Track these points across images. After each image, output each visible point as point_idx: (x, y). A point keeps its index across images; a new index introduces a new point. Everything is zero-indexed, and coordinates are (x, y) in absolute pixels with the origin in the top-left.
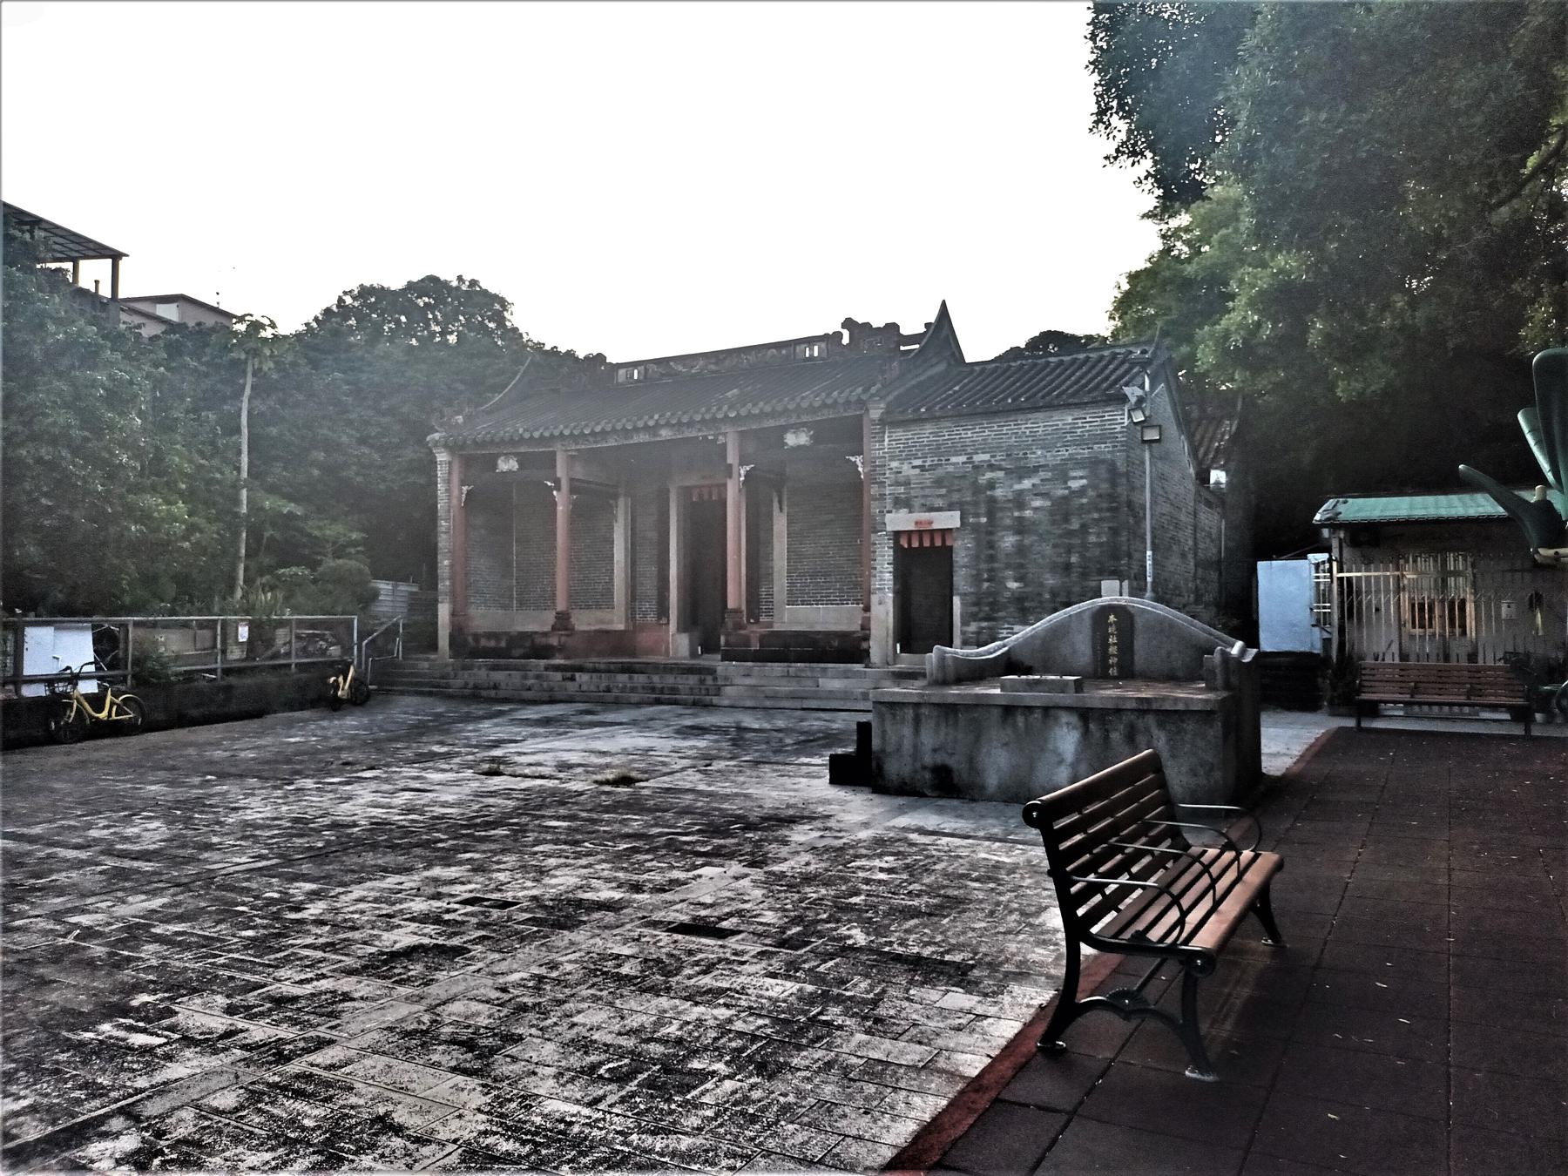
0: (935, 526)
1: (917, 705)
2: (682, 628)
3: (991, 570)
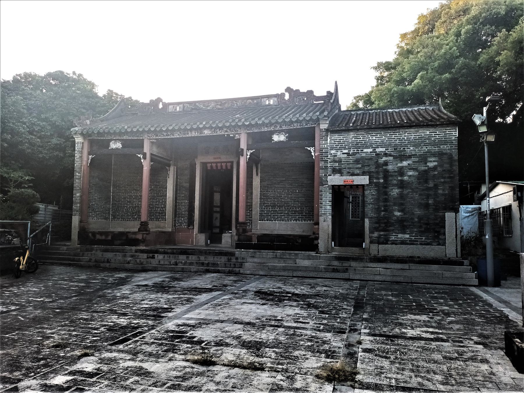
2: (201, 231)
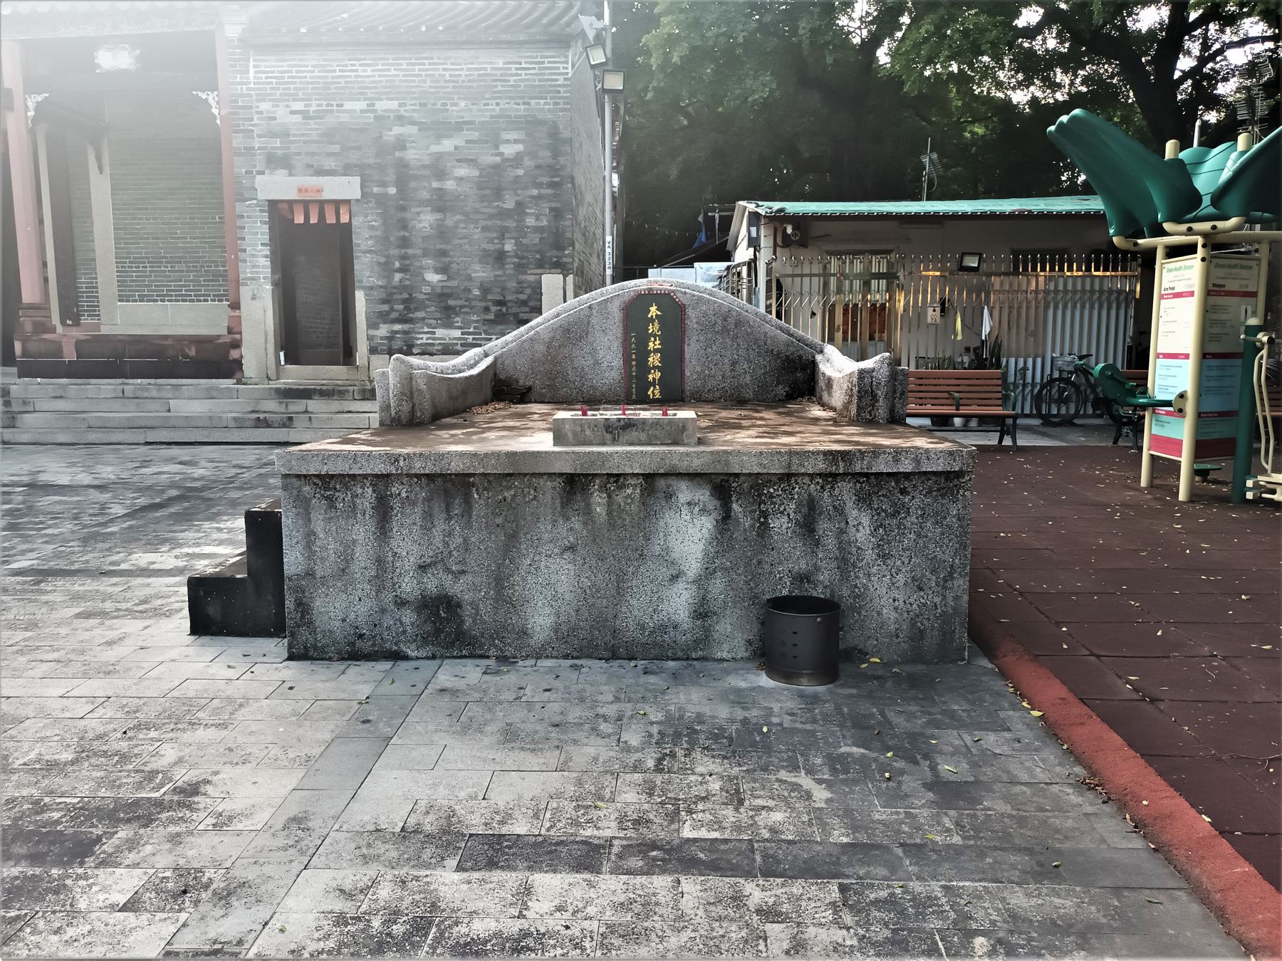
0: (327, 195)
3: (403, 257)
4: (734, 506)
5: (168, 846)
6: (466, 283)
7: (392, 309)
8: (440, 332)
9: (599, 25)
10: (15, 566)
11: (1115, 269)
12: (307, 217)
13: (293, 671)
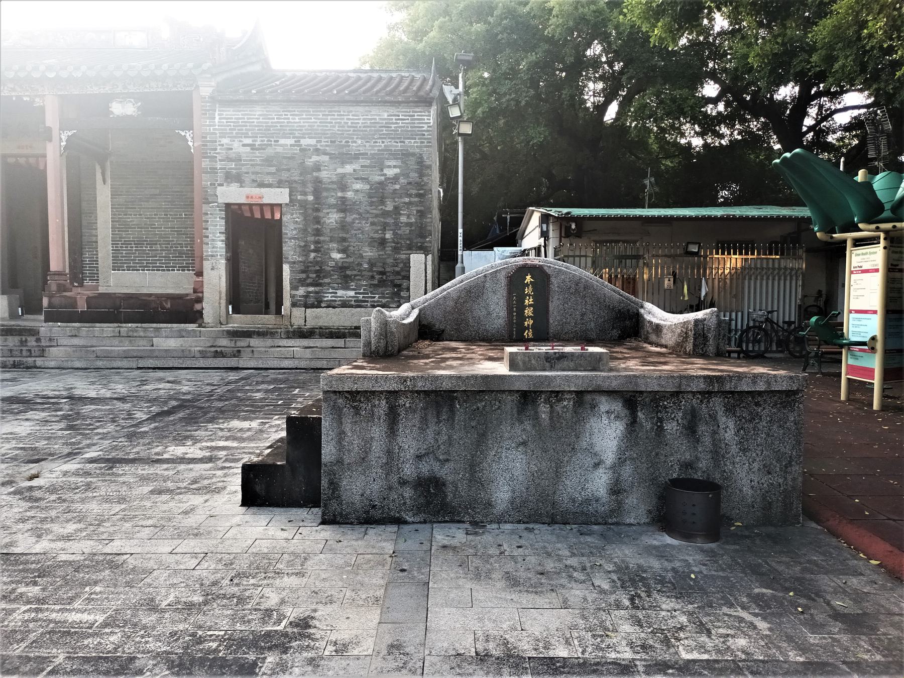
1: (393, 394)
4: (639, 414)
5: (310, 668)
6: (359, 260)
7: (308, 277)
8: (340, 293)
9: (456, 91)
10: (87, 456)
11: (753, 254)
12: (273, 215)
13: (327, 533)
